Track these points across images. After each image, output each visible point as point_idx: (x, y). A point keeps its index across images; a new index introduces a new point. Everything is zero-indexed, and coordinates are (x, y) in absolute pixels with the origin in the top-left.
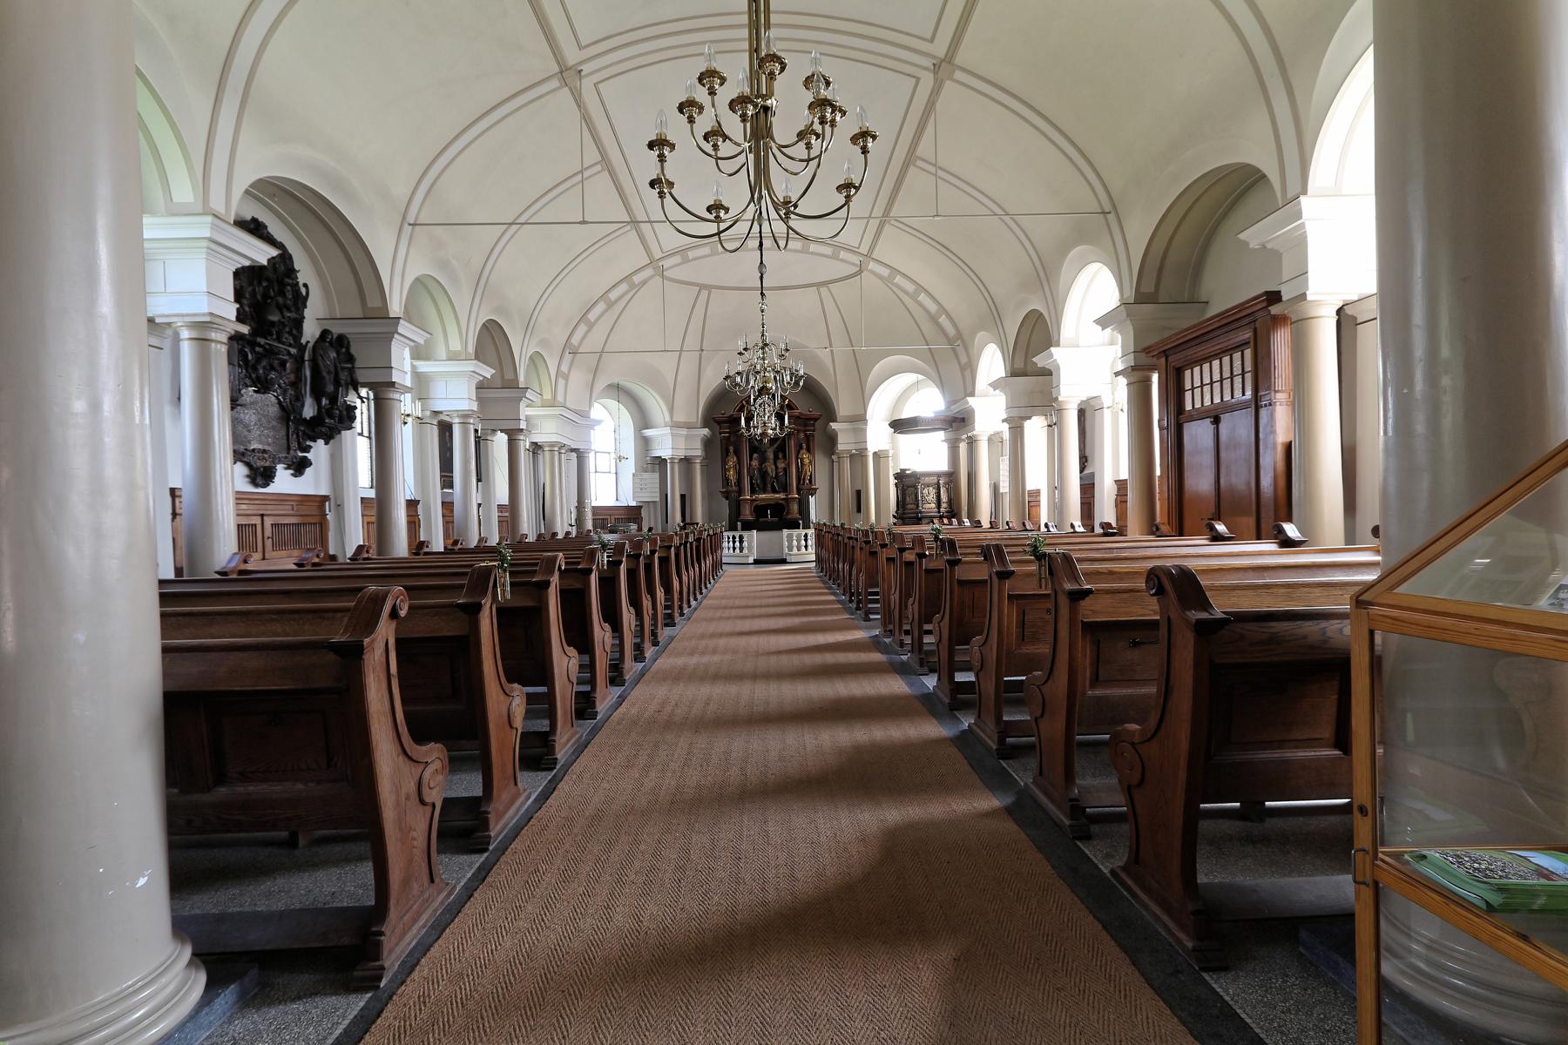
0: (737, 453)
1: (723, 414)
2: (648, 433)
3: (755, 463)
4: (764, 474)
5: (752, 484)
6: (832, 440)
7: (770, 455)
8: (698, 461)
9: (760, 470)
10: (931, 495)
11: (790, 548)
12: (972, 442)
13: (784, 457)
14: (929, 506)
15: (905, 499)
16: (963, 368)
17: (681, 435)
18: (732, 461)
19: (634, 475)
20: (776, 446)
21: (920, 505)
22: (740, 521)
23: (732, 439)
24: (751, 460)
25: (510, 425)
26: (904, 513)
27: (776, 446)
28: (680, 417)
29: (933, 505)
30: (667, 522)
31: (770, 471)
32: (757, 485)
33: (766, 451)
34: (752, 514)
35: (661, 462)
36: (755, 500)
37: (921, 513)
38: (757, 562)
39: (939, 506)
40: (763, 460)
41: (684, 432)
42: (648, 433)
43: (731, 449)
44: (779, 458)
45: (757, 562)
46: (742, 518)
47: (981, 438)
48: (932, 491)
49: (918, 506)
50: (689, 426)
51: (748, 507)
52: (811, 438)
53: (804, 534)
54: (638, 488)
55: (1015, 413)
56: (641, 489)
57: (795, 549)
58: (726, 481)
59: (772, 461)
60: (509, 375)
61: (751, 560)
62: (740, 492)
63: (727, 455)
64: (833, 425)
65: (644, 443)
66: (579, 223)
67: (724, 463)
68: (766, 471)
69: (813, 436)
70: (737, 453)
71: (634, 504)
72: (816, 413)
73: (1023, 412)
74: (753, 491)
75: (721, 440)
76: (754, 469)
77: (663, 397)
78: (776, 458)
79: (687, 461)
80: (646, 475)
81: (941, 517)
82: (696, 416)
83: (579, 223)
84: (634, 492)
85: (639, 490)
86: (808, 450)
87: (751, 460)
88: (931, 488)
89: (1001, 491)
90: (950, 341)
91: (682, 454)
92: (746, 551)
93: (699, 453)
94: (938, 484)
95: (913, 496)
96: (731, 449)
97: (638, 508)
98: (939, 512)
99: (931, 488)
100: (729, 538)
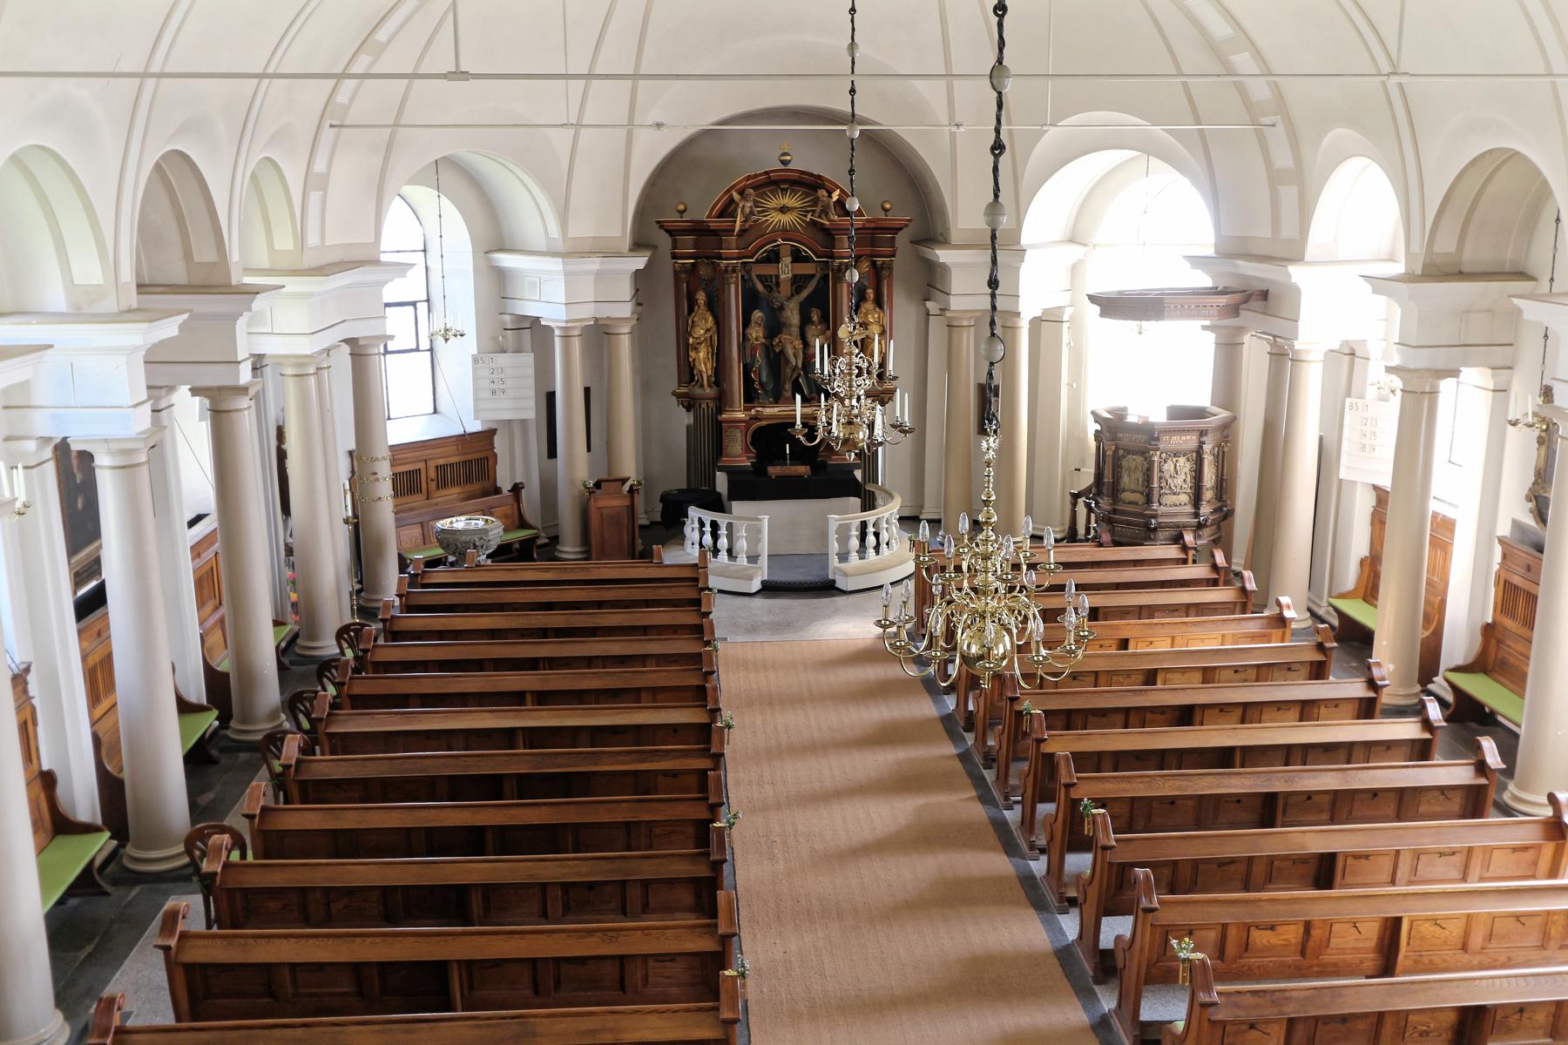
0: (716, 307)
1: (681, 212)
2: (506, 260)
3: (756, 333)
4: (776, 360)
5: (748, 382)
6: (931, 281)
7: (793, 316)
8: (626, 330)
9: (768, 349)
10: (1177, 474)
11: (843, 557)
12: (1282, 359)
13: (825, 319)
14: (1174, 503)
15: (1120, 478)
16: (1275, 179)
17: (588, 273)
18: (703, 326)
19: (475, 360)
20: (805, 294)
21: (1155, 499)
22: (721, 469)
23: (704, 271)
24: (746, 323)
25: (214, 377)
26: (1115, 511)
27: (805, 294)
28: (583, 229)
29: (1184, 498)
30: (552, 453)
31: (790, 352)
32: (761, 384)
33: (782, 308)
34: (747, 450)
35: (533, 332)
36: (755, 418)
37: (1155, 517)
38: (770, 589)
39: (1197, 500)
40: (774, 328)
41: (594, 264)
42: (506, 260)
43: (701, 297)
44: (813, 323)
45: (770, 589)
46: (725, 461)
47: (1310, 357)
48: (1184, 465)
49: (1149, 501)
50: (605, 251)
51: (739, 435)
52: (885, 273)
53: (856, 523)
54: (487, 387)
55: (1422, 360)
56: (494, 392)
57: (854, 556)
58: (688, 372)
59: (795, 330)
60: (204, 253)
61: (756, 586)
62: (722, 402)
63: (691, 311)
64: (943, 255)
65: (497, 284)
66: (444, 76)
67: (683, 333)
68: (782, 351)
69: (890, 268)
70: (716, 307)
71: (475, 426)
72: (897, 216)
73: (1441, 359)
74: (750, 397)
75: (676, 273)
76: (754, 349)
77: (546, 186)
78: (805, 321)
79: (599, 334)
80: (503, 360)
81: (1200, 526)
82: (618, 225)
83: (444, 76)
84: (476, 400)
85: (487, 394)
86: (879, 303)
87: (746, 323)
88: (1182, 460)
89: (1343, 474)
90: (1252, 111)
91: (587, 313)
92: (742, 560)
93: (626, 310)
94: (1199, 452)
95: (1140, 476)
96: (701, 297)
97: (488, 435)
98: (1197, 515)
99: (1182, 460)
100: (702, 524)
